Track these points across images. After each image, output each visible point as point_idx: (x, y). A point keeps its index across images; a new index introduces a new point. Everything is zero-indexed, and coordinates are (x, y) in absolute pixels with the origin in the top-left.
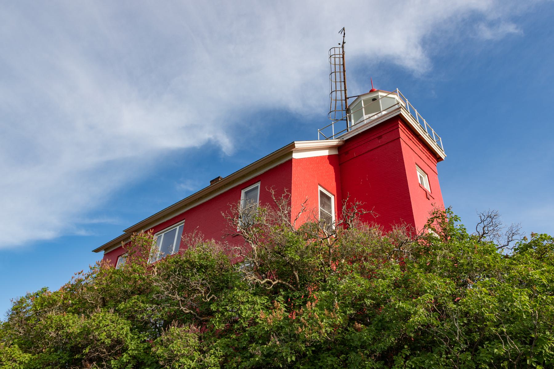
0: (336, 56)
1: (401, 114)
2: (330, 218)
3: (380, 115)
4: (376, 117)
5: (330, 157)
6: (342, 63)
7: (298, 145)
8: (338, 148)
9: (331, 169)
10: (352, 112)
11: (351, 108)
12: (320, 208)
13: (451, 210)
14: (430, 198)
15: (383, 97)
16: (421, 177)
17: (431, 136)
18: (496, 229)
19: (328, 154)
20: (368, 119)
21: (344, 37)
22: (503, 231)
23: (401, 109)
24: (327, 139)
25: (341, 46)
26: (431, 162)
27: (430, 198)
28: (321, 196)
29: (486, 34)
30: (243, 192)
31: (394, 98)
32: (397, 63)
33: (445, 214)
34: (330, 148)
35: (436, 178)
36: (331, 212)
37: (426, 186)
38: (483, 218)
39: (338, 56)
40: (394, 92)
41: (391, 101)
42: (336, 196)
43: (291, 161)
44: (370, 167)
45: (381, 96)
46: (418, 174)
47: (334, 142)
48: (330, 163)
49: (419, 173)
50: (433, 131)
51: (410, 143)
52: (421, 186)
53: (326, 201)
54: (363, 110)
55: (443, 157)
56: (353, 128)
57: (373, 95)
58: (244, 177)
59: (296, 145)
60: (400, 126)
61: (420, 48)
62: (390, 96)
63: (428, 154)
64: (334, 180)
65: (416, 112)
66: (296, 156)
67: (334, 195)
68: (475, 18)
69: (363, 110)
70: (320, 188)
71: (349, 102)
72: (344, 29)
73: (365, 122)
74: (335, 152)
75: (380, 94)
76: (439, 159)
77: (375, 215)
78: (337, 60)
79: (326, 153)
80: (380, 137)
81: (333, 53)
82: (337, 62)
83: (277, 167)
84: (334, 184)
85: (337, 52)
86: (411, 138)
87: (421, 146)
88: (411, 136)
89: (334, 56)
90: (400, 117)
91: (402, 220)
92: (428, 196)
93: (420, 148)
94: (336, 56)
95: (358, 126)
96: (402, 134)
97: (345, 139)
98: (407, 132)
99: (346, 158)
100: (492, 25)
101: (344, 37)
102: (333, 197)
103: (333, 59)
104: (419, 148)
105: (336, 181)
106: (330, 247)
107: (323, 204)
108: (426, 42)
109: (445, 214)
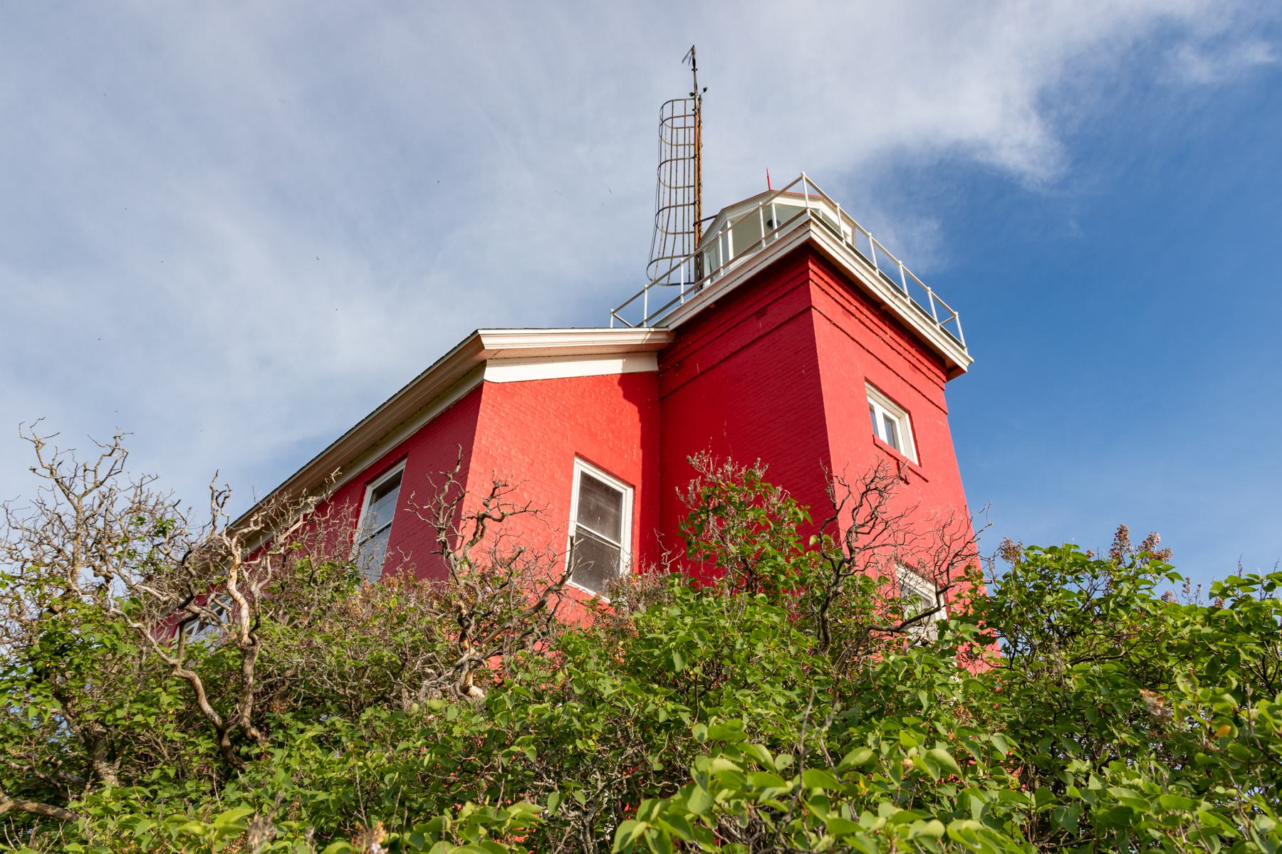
1: (811, 240)
2: (616, 554)
9: (630, 417)
14: (913, 478)
16: (887, 419)
17: (920, 305)
21: (694, 70)
23: (812, 227)
27: (913, 478)
28: (583, 490)
29: (1196, 69)
30: (369, 490)
32: (980, 157)
34: (630, 352)
35: (943, 422)
36: (617, 535)
37: (907, 450)
42: (639, 487)
46: (879, 411)
47: (639, 336)
48: (626, 396)
49: (881, 409)
50: (930, 293)
51: (851, 325)
53: (602, 503)
55: (963, 364)
58: (374, 446)
59: (484, 340)
60: (811, 275)
61: (1035, 119)
64: (637, 441)
66: (493, 374)
67: (633, 487)
68: (1169, 34)
70: (579, 467)
71: (705, 226)
74: (646, 366)
76: (951, 370)
79: (615, 367)
80: (761, 313)
83: (448, 410)
84: (637, 454)
86: (852, 309)
88: (853, 305)
90: (810, 251)
93: (887, 338)
96: (817, 297)
97: (672, 327)
98: (838, 292)
100: (1215, 45)
101: (694, 70)
102: (630, 490)
104: (882, 341)
105: (644, 445)
107: (587, 513)
108: (1044, 103)
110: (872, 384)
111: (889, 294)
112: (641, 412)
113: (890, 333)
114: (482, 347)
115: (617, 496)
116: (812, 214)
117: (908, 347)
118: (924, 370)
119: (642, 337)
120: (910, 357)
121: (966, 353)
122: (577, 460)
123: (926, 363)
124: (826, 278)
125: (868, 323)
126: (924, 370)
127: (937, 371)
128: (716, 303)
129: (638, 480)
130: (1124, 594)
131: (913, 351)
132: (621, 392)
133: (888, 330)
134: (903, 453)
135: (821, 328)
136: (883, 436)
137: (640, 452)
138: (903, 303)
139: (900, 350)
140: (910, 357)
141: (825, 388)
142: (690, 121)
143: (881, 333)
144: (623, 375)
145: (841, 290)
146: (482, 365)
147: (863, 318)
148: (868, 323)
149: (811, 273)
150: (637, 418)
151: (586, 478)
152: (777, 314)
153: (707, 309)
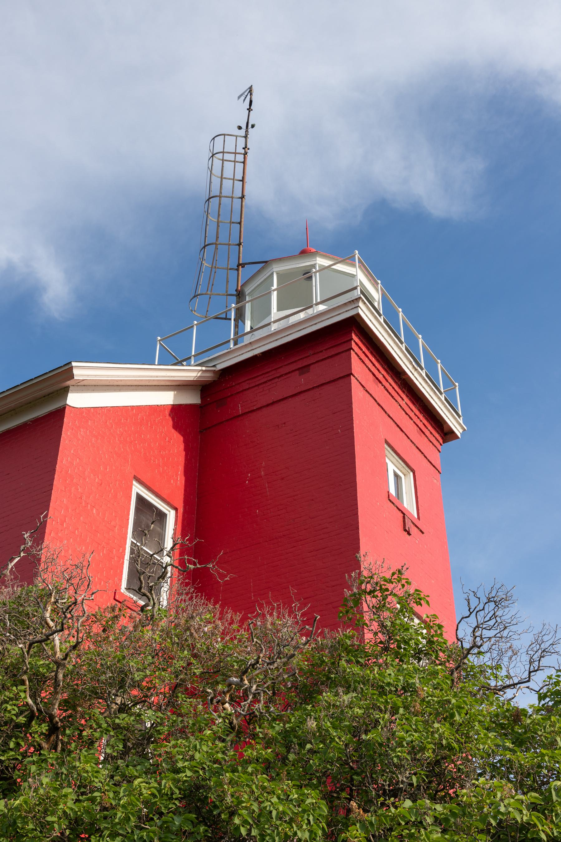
0: (227, 156)
1: (358, 314)
3: (310, 312)
4: (302, 316)
5: (177, 412)
6: (239, 176)
7: (82, 371)
8: (204, 388)
9: (175, 445)
10: (248, 299)
11: (248, 290)
12: (130, 539)
13: (406, 574)
14: (414, 530)
15: (323, 269)
16: (396, 476)
17: (432, 379)
18: (505, 633)
19: (172, 403)
20: (278, 320)
21: (249, 110)
22: (522, 642)
23: (361, 304)
24: (179, 363)
25: (242, 132)
26: (427, 440)
27: (414, 530)
28: (137, 510)
31: (353, 276)
33: (390, 586)
34: (180, 386)
37: (409, 503)
38: (474, 602)
39: (231, 157)
40: (349, 260)
41: (351, 283)
42: (181, 510)
43: (60, 412)
44: (266, 447)
45: (320, 266)
47: (191, 372)
48: (176, 427)
49: (392, 466)
51: (377, 391)
52: (394, 502)
54: (274, 296)
55: (458, 431)
56: (247, 339)
57: (304, 263)
59: (75, 372)
60: (353, 345)
62: (340, 267)
63: (422, 421)
64: (181, 468)
65: (401, 314)
66: (75, 400)
67: (176, 509)
69: (274, 296)
70: (137, 489)
72: (250, 90)
73: (274, 327)
74: (191, 399)
75: (321, 262)
76: (447, 434)
77: (222, 576)
78: (229, 166)
79: (167, 398)
80: (304, 370)
81: (218, 148)
82: (228, 173)
84: (179, 480)
85: (230, 147)
86: (380, 377)
87: (406, 401)
88: (382, 374)
89: (220, 156)
90: (355, 324)
91: (293, 591)
92: (409, 525)
93: (403, 403)
94: (227, 156)
95: (258, 335)
96: (357, 366)
97: (220, 367)
98: (372, 361)
99: (212, 417)
101: (249, 110)
102: (173, 512)
103: (217, 163)
104: (399, 406)
106: (58, 664)
107: (140, 531)
109: (390, 586)
110: (389, 445)
111: (410, 367)
112: (185, 442)
113: (406, 400)
114: (72, 376)
115: (162, 516)
116: (362, 292)
117: (418, 413)
118: (428, 433)
119: (194, 374)
120: (418, 422)
121: (461, 422)
122: (134, 482)
123: (430, 428)
124: (364, 349)
125: (391, 389)
126: (428, 433)
127: (437, 435)
128: (264, 353)
129: (180, 505)
130: (257, 810)
131: (421, 416)
132: (171, 423)
133: (404, 396)
134: (405, 505)
135: (357, 393)
136: (392, 491)
137: (183, 478)
138: (421, 375)
139: (412, 414)
140: (418, 422)
141: (357, 448)
142: (240, 158)
143: (399, 399)
144: (173, 406)
145: (373, 360)
146: (65, 391)
147: (387, 385)
148: (391, 389)
149: (353, 343)
150: (182, 447)
151: (140, 499)
152: (319, 373)
153: (254, 358)
